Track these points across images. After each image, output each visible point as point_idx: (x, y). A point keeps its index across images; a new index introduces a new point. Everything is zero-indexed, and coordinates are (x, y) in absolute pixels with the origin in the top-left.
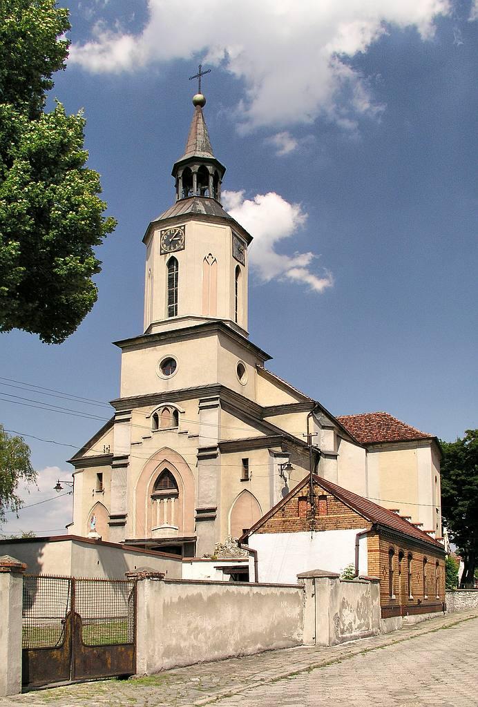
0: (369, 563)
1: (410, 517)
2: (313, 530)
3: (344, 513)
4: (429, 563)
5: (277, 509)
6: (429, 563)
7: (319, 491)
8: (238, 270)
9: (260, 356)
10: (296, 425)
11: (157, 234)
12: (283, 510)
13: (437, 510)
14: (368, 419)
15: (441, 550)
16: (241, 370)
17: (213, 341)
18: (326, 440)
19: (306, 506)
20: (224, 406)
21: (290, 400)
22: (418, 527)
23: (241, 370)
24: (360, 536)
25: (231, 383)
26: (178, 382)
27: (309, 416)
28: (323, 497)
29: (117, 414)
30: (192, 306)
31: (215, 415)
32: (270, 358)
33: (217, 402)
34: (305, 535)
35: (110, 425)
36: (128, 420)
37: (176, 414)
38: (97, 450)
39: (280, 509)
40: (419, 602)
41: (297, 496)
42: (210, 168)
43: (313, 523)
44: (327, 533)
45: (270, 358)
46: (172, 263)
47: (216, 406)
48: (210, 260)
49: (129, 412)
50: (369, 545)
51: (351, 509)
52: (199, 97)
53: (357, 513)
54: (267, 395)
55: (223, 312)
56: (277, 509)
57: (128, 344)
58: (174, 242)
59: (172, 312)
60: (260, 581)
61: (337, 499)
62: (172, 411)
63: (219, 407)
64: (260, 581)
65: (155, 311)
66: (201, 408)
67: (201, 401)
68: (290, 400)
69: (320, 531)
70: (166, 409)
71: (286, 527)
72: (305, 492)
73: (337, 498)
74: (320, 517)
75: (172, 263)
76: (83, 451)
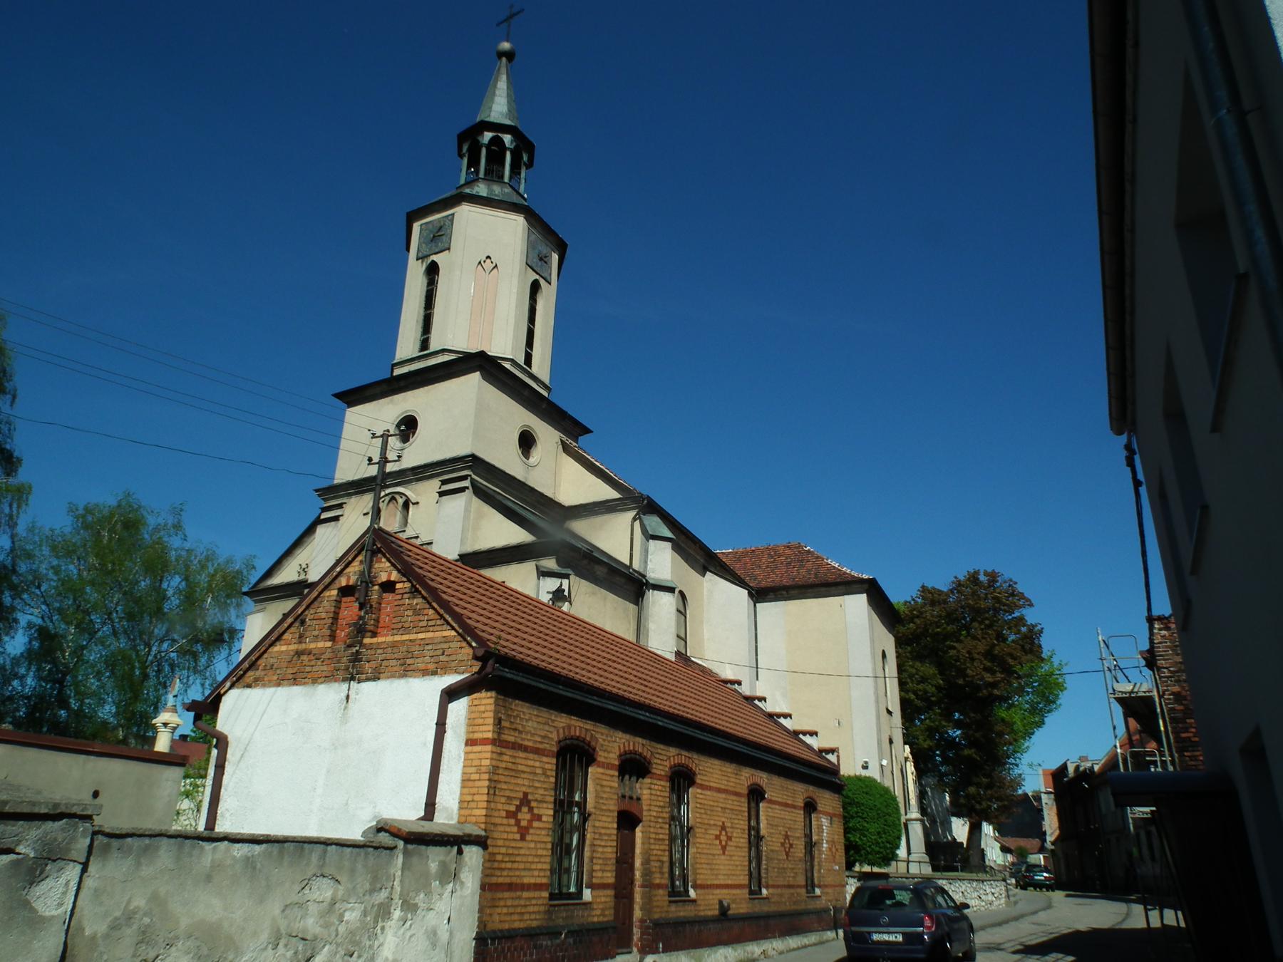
0: (466, 781)
1: (790, 716)
2: (352, 679)
3: (426, 629)
4: (770, 802)
5: (290, 620)
6: (770, 802)
7: (385, 570)
8: (535, 287)
9: (572, 429)
10: (615, 537)
11: (416, 227)
12: (303, 623)
13: (889, 712)
14: (773, 552)
15: (826, 777)
16: (527, 441)
17: (474, 379)
18: (661, 562)
19: (350, 610)
20: (480, 492)
21: (610, 493)
22: (782, 720)
23: (527, 441)
24: (450, 694)
25: (507, 459)
26: (416, 454)
27: (634, 519)
28: (389, 587)
29: (325, 510)
30: (453, 335)
31: (462, 504)
32: (587, 431)
33: (466, 483)
34: (329, 694)
35: (310, 530)
36: (336, 519)
37: (406, 505)
38: (288, 574)
39: (295, 620)
40: (724, 911)
41: (337, 584)
42: (507, 139)
43: (356, 658)
44: (382, 685)
45: (587, 431)
46: (433, 270)
47: (462, 490)
48: (488, 265)
49: (340, 506)
50: (472, 723)
51: (442, 617)
52: (506, 46)
53: (453, 628)
54: (570, 483)
55: (503, 343)
56: (290, 620)
57: (355, 396)
58: (439, 238)
59: (425, 344)
60: (222, 827)
61: (414, 592)
62: (401, 501)
63: (469, 492)
64: (222, 827)
65: (407, 346)
66: (442, 494)
67: (444, 482)
68: (610, 493)
69: (368, 679)
70: (393, 499)
71: (297, 676)
72: (352, 575)
73: (417, 590)
74: (380, 639)
75: (433, 270)
76: (804, 733)
